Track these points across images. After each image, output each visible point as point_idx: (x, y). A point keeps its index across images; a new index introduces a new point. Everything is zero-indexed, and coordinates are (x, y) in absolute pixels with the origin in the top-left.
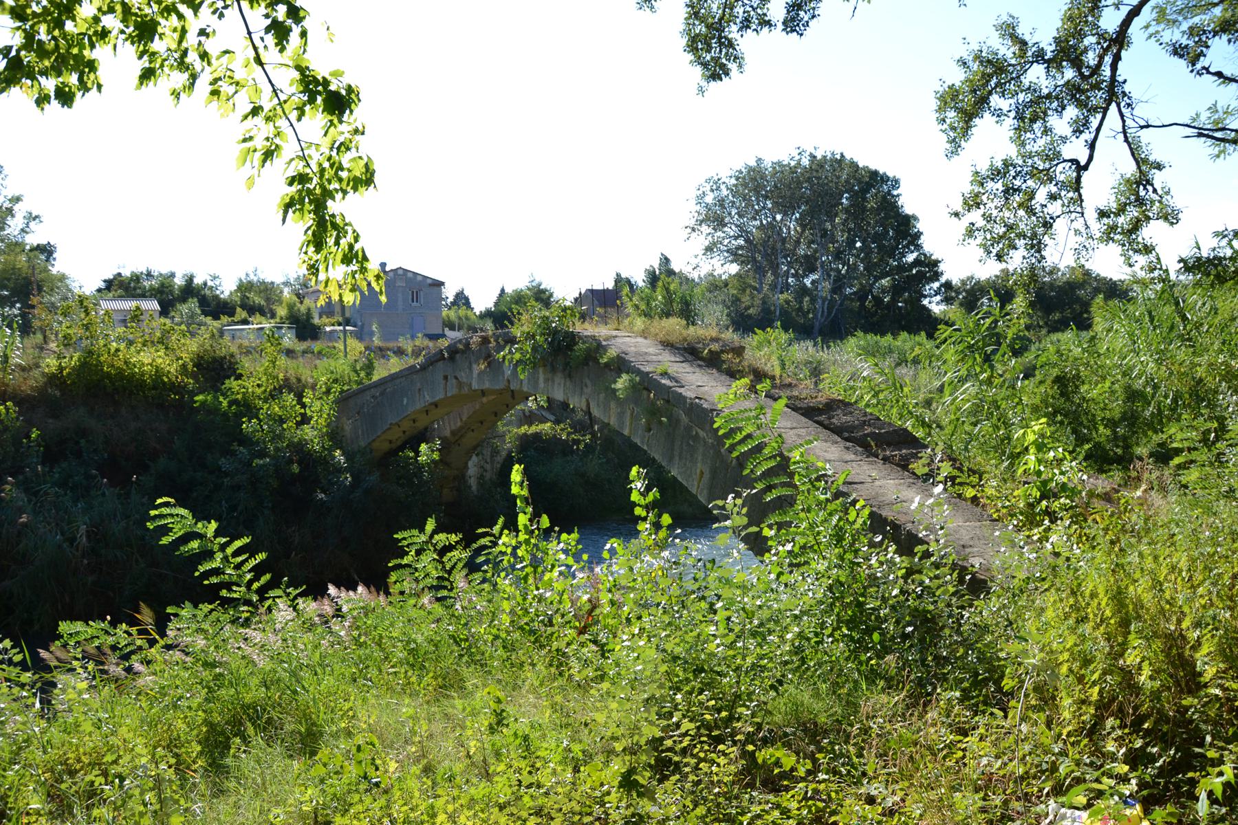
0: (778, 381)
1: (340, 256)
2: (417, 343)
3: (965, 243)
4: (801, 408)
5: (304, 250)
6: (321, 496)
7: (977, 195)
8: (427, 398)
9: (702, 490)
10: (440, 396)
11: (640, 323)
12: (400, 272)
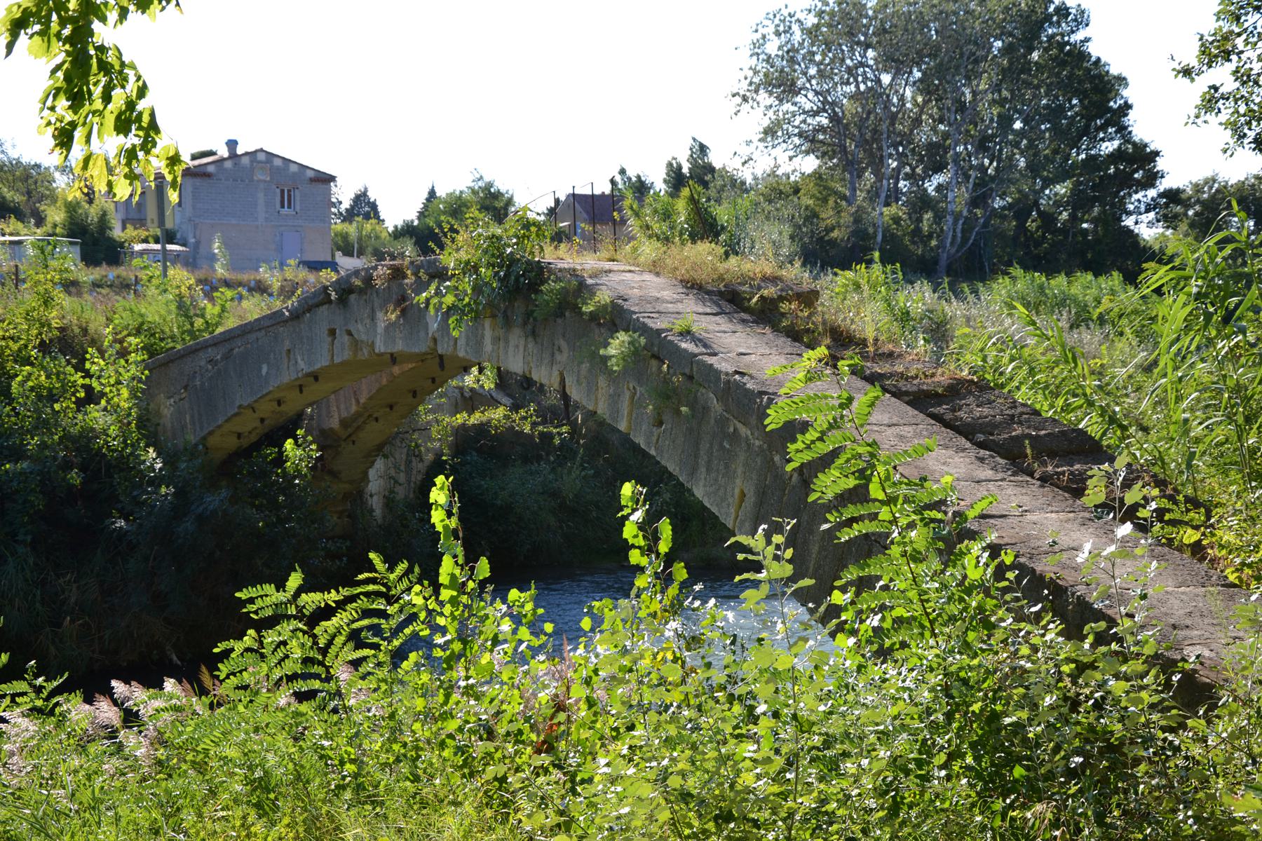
0: (871, 349)
1: (110, 120)
2: (289, 274)
3: (1199, 121)
4: (907, 393)
5: (49, 103)
6: (121, 523)
7: (1226, 38)
8: (302, 364)
9: (742, 522)
10: (322, 362)
11: (649, 250)
12: (261, 157)
